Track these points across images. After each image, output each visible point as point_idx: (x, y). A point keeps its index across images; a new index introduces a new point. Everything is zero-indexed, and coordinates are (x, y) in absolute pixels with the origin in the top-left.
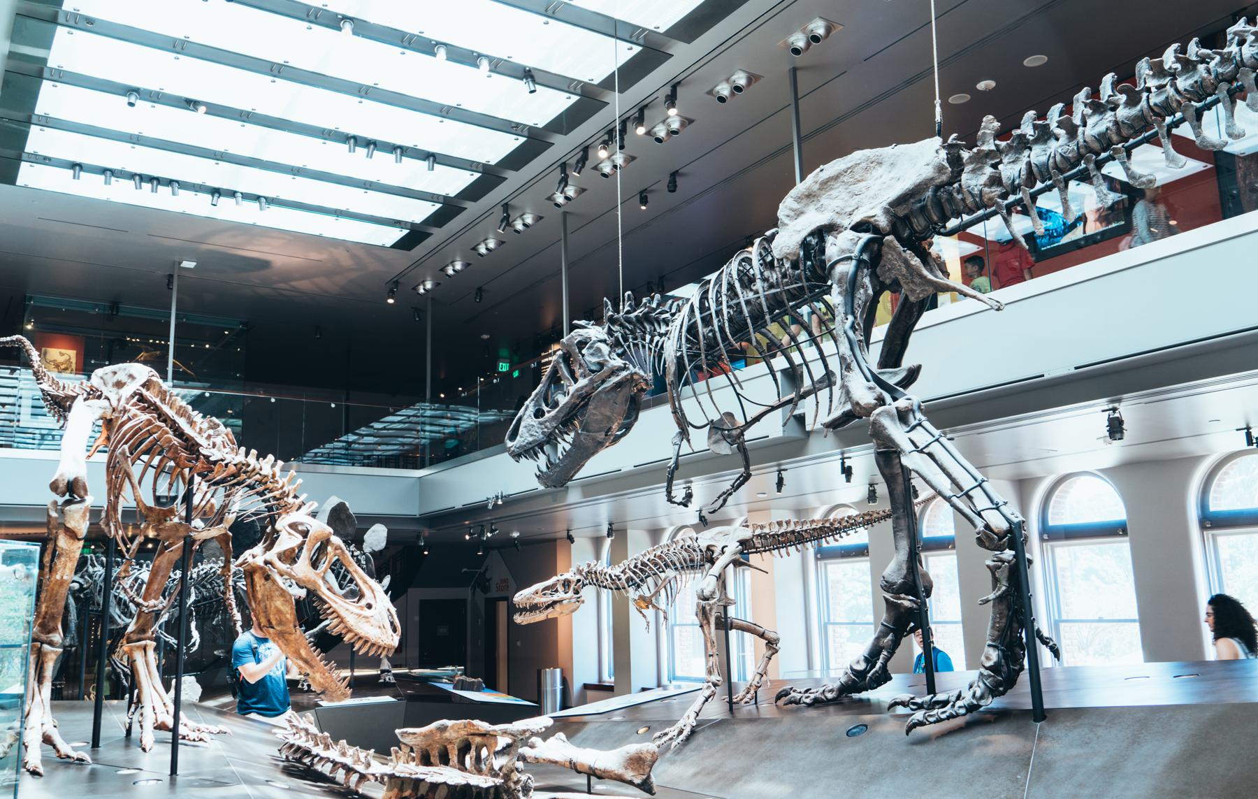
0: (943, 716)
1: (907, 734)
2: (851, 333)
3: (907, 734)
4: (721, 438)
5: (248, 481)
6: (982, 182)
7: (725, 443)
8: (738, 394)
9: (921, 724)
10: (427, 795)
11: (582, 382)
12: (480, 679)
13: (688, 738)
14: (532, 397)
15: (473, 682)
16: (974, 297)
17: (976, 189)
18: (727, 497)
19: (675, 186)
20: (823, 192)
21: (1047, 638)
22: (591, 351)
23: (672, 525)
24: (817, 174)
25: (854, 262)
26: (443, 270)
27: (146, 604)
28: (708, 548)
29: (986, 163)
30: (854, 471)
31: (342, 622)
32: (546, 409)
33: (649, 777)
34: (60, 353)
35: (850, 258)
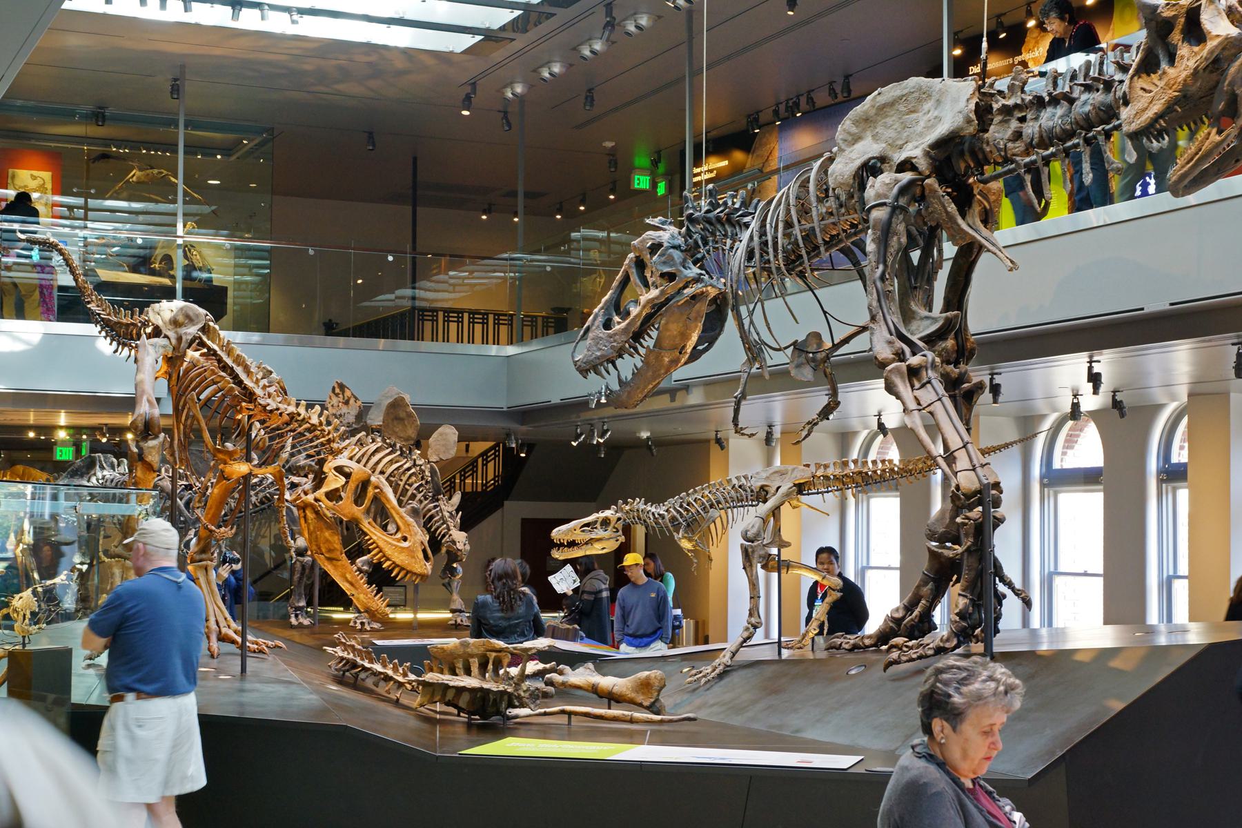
0: (914, 656)
1: (885, 671)
2: (879, 284)
3: (885, 671)
4: (804, 361)
5: (299, 430)
6: (1007, 137)
8: (825, 313)
9: (897, 662)
10: (453, 700)
11: (654, 293)
12: (576, 626)
14: (601, 305)
15: (568, 629)
16: (995, 254)
17: (1002, 143)
18: (812, 428)
20: (879, 118)
21: (1019, 590)
22: (663, 259)
23: (866, 428)
24: (875, 97)
27: (217, 531)
28: (762, 487)
29: (1012, 116)
30: (1002, 390)
31: (381, 551)
33: (657, 700)
34: (32, 175)
35: (884, 204)
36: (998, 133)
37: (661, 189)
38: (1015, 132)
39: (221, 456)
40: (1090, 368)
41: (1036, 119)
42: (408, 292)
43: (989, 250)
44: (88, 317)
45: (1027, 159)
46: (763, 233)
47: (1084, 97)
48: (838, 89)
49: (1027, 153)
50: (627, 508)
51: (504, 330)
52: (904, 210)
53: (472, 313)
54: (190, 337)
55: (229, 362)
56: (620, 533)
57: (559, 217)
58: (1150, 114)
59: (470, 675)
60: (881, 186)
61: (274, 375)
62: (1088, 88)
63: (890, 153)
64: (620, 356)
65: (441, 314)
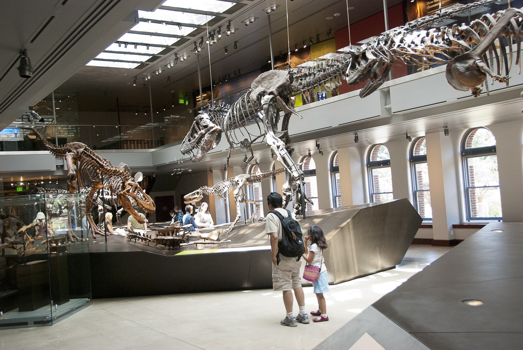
2: (267, 124)
7: (245, 148)
8: (248, 133)
13: (232, 231)
19: (236, 47)
24: (261, 76)
25: (268, 105)
26: (154, 72)
32: (192, 139)
36: (294, 83)
37: (187, 103)
38: (300, 83)
39: (95, 183)
40: (316, 143)
41: (305, 79)
42: (119, 137)
43: (293, 113)
44: (46, 149)
45: (303, 90)
46: (233, 113)
47: (318, 73)
48: (237, 73)
49: (303, 88)
50: (203, 189)
51: (139, 145)
52: (272, 105)
53: (137, 141)
54: (81, 152)
55: (95, 158)
56: (202, 195)
57: (158, 112)
58: (354, 78)
59: (169, 236)
60: (267, 98)
61: (107, 160)
62: (319, 71)
63: (266, 90)
64: (193, 149)
65: (129, 142)
